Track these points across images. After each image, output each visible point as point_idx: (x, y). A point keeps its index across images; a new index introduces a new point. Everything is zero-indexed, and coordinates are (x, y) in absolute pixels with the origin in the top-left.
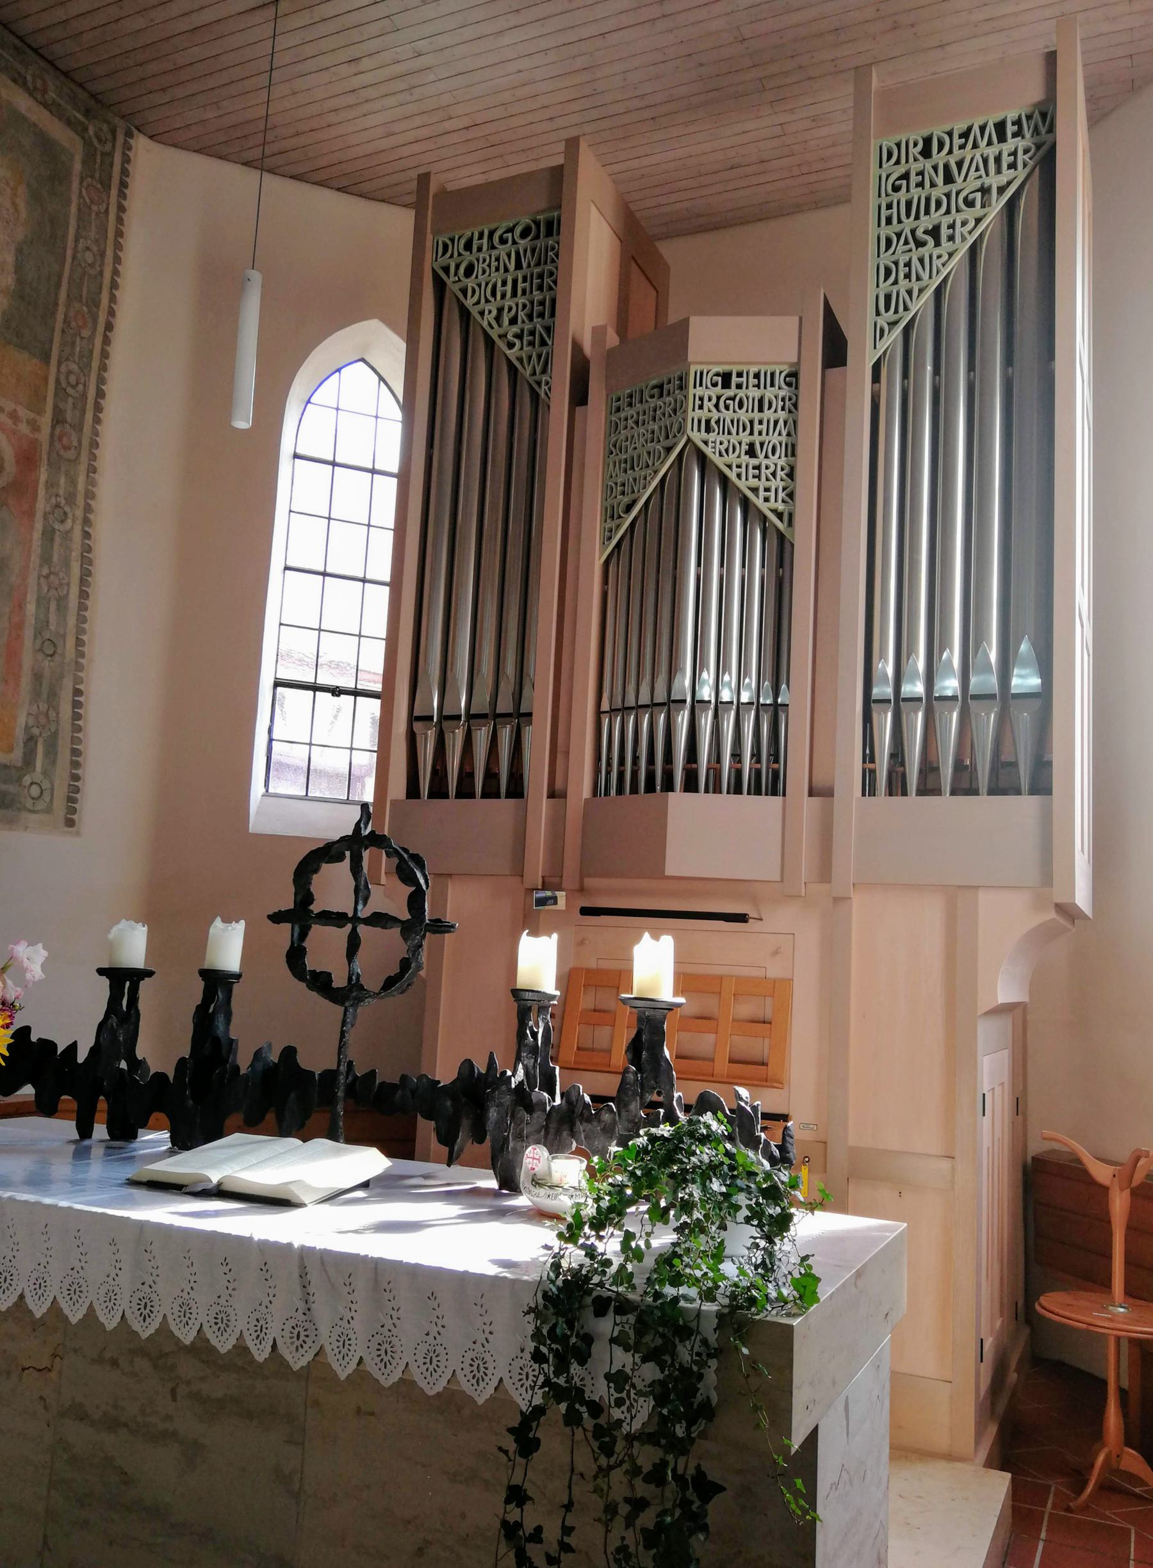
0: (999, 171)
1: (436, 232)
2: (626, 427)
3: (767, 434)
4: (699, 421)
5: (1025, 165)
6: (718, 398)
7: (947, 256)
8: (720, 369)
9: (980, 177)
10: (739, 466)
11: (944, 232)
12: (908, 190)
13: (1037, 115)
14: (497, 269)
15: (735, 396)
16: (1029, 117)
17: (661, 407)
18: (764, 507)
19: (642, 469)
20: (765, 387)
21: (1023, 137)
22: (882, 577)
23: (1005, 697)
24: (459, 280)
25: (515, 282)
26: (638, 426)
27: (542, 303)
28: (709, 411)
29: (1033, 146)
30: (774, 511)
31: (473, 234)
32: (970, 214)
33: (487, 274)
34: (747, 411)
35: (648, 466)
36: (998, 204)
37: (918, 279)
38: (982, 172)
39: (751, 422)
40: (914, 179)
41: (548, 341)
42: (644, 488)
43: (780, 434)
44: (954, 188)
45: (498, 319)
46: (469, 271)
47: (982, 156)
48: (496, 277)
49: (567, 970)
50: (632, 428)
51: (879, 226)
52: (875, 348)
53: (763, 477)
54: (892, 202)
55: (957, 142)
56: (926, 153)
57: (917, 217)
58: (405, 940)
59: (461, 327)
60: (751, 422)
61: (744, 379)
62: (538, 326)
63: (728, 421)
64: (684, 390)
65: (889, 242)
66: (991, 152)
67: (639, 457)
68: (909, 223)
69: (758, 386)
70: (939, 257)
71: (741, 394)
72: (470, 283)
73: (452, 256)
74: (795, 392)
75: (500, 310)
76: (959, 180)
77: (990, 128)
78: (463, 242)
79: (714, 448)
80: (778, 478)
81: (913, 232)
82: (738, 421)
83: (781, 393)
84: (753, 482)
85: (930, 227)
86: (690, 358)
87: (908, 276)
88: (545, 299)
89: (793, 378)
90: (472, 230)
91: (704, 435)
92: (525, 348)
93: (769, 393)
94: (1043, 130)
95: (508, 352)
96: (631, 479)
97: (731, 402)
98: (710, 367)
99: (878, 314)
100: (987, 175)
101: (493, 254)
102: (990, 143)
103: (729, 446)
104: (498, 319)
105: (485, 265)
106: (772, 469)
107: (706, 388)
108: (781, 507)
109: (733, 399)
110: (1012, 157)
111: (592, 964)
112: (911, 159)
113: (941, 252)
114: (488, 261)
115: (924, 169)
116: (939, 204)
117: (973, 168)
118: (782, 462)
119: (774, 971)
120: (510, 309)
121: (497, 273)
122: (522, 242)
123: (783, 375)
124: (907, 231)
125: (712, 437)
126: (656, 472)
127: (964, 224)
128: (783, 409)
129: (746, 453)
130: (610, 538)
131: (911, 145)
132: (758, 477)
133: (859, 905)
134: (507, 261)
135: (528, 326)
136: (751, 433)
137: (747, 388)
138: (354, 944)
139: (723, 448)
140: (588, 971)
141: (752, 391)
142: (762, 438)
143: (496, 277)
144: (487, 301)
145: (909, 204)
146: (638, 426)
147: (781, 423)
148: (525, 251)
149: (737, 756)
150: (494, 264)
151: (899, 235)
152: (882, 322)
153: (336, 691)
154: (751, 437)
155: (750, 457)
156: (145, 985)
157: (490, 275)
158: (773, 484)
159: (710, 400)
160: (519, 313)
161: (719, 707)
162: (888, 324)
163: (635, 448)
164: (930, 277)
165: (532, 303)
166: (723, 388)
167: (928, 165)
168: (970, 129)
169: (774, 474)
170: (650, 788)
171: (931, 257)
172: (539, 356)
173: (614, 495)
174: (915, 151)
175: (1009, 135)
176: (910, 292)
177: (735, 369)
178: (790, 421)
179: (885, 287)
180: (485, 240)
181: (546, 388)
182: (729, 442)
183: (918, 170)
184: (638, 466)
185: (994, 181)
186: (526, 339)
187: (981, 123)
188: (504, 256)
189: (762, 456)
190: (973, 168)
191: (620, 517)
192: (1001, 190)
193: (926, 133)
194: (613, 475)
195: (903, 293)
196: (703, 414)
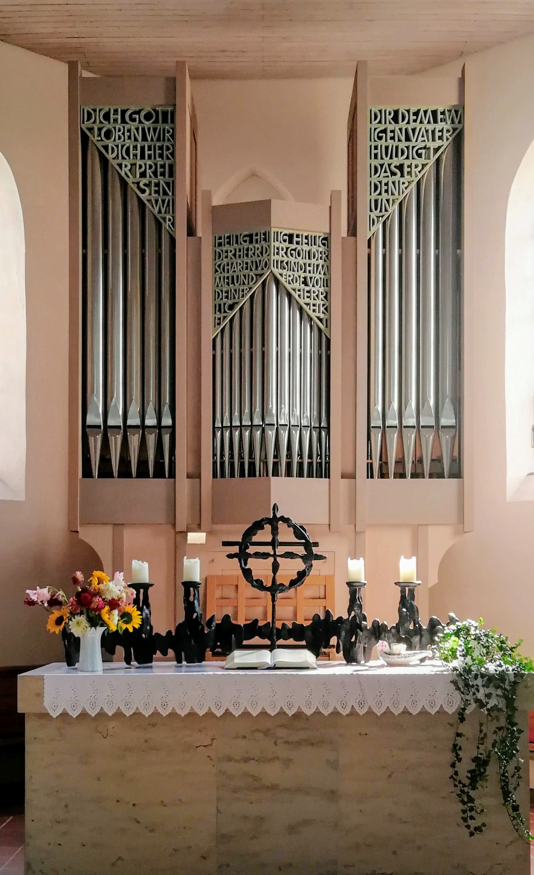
0: (434, 140)
2: (227, 257)
4: (277, 262)
5: (447, 139)
6: (287, 249)
9: (424, 141)
11: (406, 170)
12: (386, 141)
13: (453, 111)
14: (129, 138)
15: (296, 248)
17: (251, 249)
19: (240, 285)
23: (438, 427)
24: (102, 140)
25: (143, 148)
26: (236, 258)
27: (163, 166)
30: (318, 318)
31: (110, 109)
32: (419, 161)
33: (123, 139)
34: (302, 258)
35: (244, 284)
36: (433, 159)
38: (425, 138)
40: (390, 135)
41: (169, 192)
42: (243, 296)
44: (411, 144)
46: (108, 134)
47: (425, 128)
48: (129, 143)
49: (204, 577)
50: (231, 258)
51: (371, 158)
57: (391, 158)
58: (305, 564)
59: (101, 172)
65: (376, 169)
66: (430, 127)
67: (238, 276)
68: (387, 160)
69: (307, 244)
70: (403, 183)
71: (299, 247)
72: (110, 144)
73: (95, 122)
76: (414, 140)
77: (429, 113)
78: (102, 113)
81: (389, 165)
82: (298, 263)
84: (307, 300)
85: (398, 165)
88: (165, 164)
89: (326, 240)
90: (111, 107)
92: (153, 195)
93: (314, 249)
94: (456, 121)
95: (141, 196)
96: (232, 290)
99: (371, 211)
100: (428, 141)
101: (126, 127)
103: (294, 278)
105: (120, 133)
108: (322, 316)
112: (388, 122)
118: (322, 290)
120: (140, 167)
124: (386, 165)
126: (250, 288)
127: (416, 166)
130: (219, 324)
131: (387, 114)
133: (368, 534)
134: (136, 134)
135: (154, 180)
136: (305, 272)
137: (302, 245)
138: (275, 567)
139: (290, 279)
143: (129, 143)
145: (387, 148)
146: (236, 258)
147: (320, 267)
148: (149, 129)
150: (127, 134)
151: (382, 166)
152: (374, 215)
156: (150, 590)
157: (124, 141)
158: (318, 302)
159: (282, 250)
163: (234, 271)
165: (156, 165)
166: (289, 243)
168: (419, 111)
171: (399, 182)
172: (163, 201)
174: (389, 118)
176: (388, 201)
177: (295, 233)
178: (325, 266)
179: (374, 196)
184: (237, 283)
186: (153, 188)
187: (425, 109)
188: (133, 130)
189: (311, 285)
195: (384, 201)
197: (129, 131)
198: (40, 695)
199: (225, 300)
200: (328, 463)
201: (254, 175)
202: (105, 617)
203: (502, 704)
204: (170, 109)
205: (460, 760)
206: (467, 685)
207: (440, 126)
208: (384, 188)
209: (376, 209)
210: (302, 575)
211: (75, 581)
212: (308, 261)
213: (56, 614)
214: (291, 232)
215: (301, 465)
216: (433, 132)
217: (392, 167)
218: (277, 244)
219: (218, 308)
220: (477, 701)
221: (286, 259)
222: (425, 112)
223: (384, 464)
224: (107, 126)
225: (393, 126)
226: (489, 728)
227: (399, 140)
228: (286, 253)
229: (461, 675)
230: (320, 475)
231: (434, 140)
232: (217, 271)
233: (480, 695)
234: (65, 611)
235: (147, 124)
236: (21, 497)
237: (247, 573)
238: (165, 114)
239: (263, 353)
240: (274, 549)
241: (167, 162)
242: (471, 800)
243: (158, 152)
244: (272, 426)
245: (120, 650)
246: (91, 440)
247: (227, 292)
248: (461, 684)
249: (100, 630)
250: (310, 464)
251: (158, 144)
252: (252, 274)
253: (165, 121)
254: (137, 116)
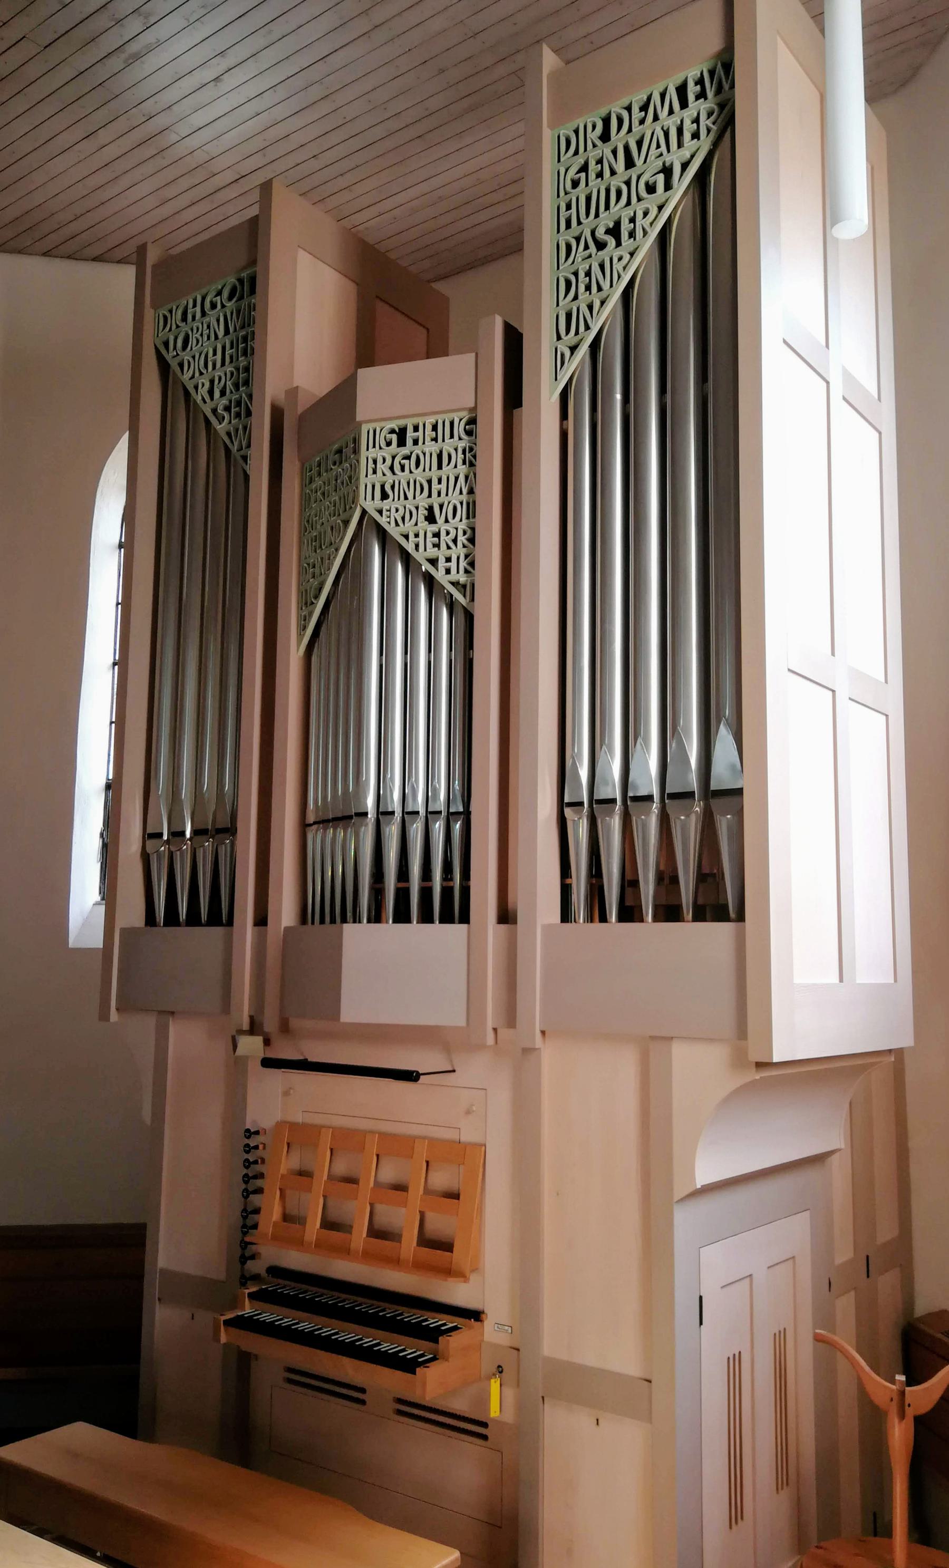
1: (155, 306)
3: (447, 495)
5: (709, 130)
7: (628, 256)
8: (394, 425)
10: (417, 536)
11: (625, 227)
14: (209, 338)
21: (706, 99)
22: (574, 656)
24: (178, 355)
28: (384, 475)
30: (455, 584)
32: (651, 202)
34: (424, 470)
36: (682, 183)
37: (600, 289)
39: (429, 482)
40: (593, 168)
42: (329, 569)
43: (461, 493)
44: (634, 172)
45: (211, 392)
47: (662, 128)
51: (558, 231)
52: (556, 379)
53: (443, 546)
54: (571, 201)
55: (637, 114)
56: (605, 137)
60: (429, 482)
61: (420, 434)
62: (244, 395)
64: (357, 454)
66: (672, 123)
75: (212, 382)
76: (639, 162)
77: (672, 94)
78: (180, 312)
79: (389, 517)
80: (460, 544)
81: (593, 233)
84: (432, 552)
86: (359, 418)
90: (193, 296)
91: (378, 502)
92: (233, 422)
96: (319, 559)
97: (406, 462)
98: (383, 424)
99: (559, 338)
100: (669, 151)
101: (204, 321)
102: (671, 112)
104: (211, 392)
105: (198, 335)
106: (452, 535)
107: (380, 448)
108: (462, 578)
109: (408, 457)
110: (695, 125)
111: (299, 1118)
113: (621, 253)
114: (200, 330)
115: (602, 157)
118: (462, 526)
119: (467, 1136)
122: (228, 304)
123: (463, 423)
124: (587, 233)
125: (386, 505)
128: (464, 463)
132: (437, 546)
135: (235, 397)
141: (428, 446)
142: (440, 500)
144: (201, 374)
151: (578, 239)
155: (429, 523)
157: (202, 345)
160: (227, 383)
161: (432, 814)
164: (611, 286)
165: (238, 369)
169: (455, 541)
170: (333, 921)
174: (594, 135)
180: (198, 309)
182: (405, 508)
184: (324, 545)
185: (675, 158)
191: (313, 603)
192: (685, 166)
193: (603, 112)
196: (378, 479)
209: (568, 331)
214: (401, 423)
215: (426, 893)
218: (372, 453)
225: (600, 149)
228: (392, 468)
230: (447, 918)
244: (687, 802)
252: (340, 521)
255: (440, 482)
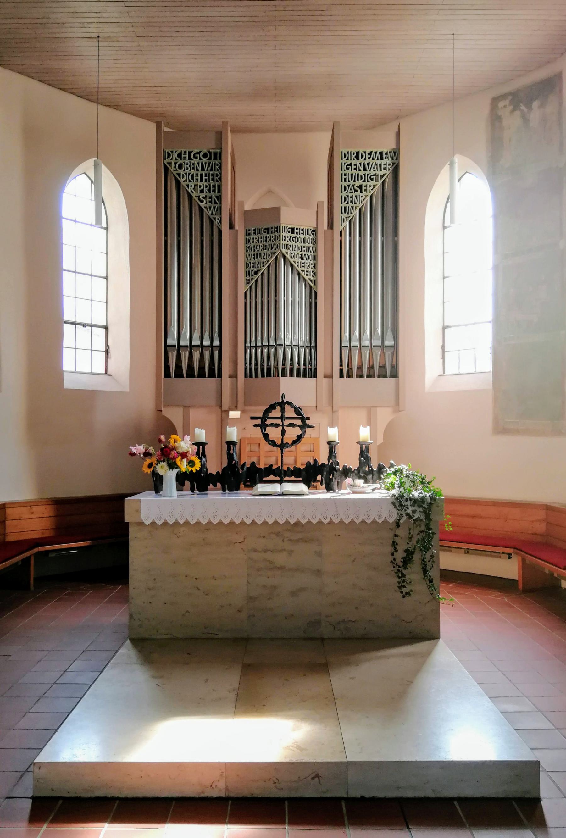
0: (381, 170)
2: (253, 242)
4: (284, 245)
5: (389, 170)
6: (291, 237)
8: (291, 227)
9: (375, 171)
11: (364, 188)
12: (351, 170)
14: (193, 169)
16: (390, 152)
17: (269, 237)
18: (306, 277)
20: (305, 235)
23: (383, 347)
24: (176, 170)
26: (259, 242)
27: (214, 186)
28: (288, 242)
29: (392, 164)
30: (310, 279)
31: (181, 151)
32: (372, 183)
35: (264, 258)
36: (380, 182)
37: (355, 203)
38: (376, 169)
40: (354, 167)
41: (218, 202)
44: (367, 173)
46: (180, 166)
48: (193, 172)
49: (239, 438)
50: (256, 243)
57: (354, 181)
62: (213, 195)
63: (294, 246)
65: (345, 187)
68: (352, 183)
69: (303, 234)
72: (182, 172)
74: (316, 237)
78: (177, 154)
81: (353, 185)
83: (311, 237)
85: (359, 185)
87: (352, 201)
88: (215, 185)
89: (314, 232)
93: (307, 237)
94: (395, 158)
95: (201, 204)
96: (257, 262)
99: (342, 213)
102: (378, 159)
105: (188, 166)
108: (312, 278)
109: (295, 238)
116: (362, 178)
117: (373, 167)
118: (312, 262)
121: (193, 171)
124: (351, 185)
127: (370, 186)
129: (300, 258)
130: (248, 283)
135: (209, 195)
136: (301, 251)
138: (283, 433)
139: (293, 255)
140: (248, 438)
143: (193, 172)
145: (352, 175)
146: (259, 242)
148: (206, 163)
149: (299, 363)
151: (349, 186)
153: (84, 325)
154: (301, 252)
158: (309, 270)
159: (288, 238)
162: (346, 217)
165: (210, 185)
166: (292, 233)
167: (358, 162)
168: (371, 152)
172: (214, 208)
173: (249, 266)
174: (353, 156)
175: (384, 158)
176: (352, 207)
178: (314, 248)
179: (344, 204)
180: (187, 156)
181: (218, 221)
183: (355, 163)
184: (260, 258)
186: (208, 200)
187: (375, 151)
188: (196, 164)
189: (305, 259)
190: (373, 167)
191: (252, 276)
194: (249, 259)
197: (193, 164)
198: (138, 511)
199: (252, 268)
200: (316, 369)
201: (270, 192)
202: (179, 463)
203: (423, 517)
204: (218, 151)
205: (397, 551)
206: (401, 505)
207: (384, 161)
208: (350, 199)
210: (299, 437)
211: (160, 441)
212: (303, 245)
213: (148, 461)
214: (293, 226)
216: (380, 165)
217: (355, 187)
219: (248, 273)
220: (407, 515)
221: (289, 243)
222: (376, 153)
223: (350, 369)
224: (180, 161)
226: (415, 532)
227: (360, 170)
228: (290, 240)
229: (397, 499)
231: (381, 170)
232: (247, 250)
233: (409, 511)
234: (154, 460)
235: (204, 160)
236: (127, 389)
237: (266, 436)
238: (215, 154)
239: (276, 301)
240: (282, 421)
241: (217, 184)
242: (404, 575)
243: (211, 177)
245: (188, 484)
246: (170, 354)
247: (253, 264)
248: (397, 505)
249: (175, 471)
250: (305, 369)
251: (211, 172)
253: (215, 158)
254: (198, 155)
255: (261, 238)
